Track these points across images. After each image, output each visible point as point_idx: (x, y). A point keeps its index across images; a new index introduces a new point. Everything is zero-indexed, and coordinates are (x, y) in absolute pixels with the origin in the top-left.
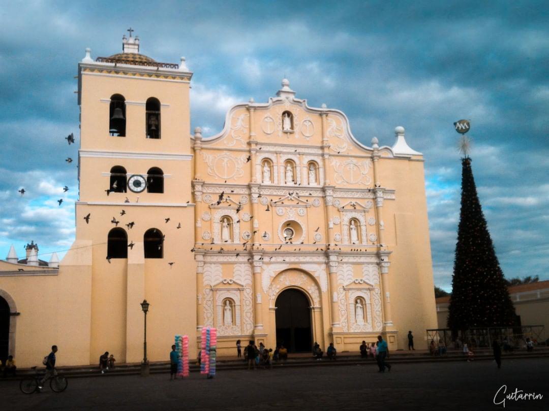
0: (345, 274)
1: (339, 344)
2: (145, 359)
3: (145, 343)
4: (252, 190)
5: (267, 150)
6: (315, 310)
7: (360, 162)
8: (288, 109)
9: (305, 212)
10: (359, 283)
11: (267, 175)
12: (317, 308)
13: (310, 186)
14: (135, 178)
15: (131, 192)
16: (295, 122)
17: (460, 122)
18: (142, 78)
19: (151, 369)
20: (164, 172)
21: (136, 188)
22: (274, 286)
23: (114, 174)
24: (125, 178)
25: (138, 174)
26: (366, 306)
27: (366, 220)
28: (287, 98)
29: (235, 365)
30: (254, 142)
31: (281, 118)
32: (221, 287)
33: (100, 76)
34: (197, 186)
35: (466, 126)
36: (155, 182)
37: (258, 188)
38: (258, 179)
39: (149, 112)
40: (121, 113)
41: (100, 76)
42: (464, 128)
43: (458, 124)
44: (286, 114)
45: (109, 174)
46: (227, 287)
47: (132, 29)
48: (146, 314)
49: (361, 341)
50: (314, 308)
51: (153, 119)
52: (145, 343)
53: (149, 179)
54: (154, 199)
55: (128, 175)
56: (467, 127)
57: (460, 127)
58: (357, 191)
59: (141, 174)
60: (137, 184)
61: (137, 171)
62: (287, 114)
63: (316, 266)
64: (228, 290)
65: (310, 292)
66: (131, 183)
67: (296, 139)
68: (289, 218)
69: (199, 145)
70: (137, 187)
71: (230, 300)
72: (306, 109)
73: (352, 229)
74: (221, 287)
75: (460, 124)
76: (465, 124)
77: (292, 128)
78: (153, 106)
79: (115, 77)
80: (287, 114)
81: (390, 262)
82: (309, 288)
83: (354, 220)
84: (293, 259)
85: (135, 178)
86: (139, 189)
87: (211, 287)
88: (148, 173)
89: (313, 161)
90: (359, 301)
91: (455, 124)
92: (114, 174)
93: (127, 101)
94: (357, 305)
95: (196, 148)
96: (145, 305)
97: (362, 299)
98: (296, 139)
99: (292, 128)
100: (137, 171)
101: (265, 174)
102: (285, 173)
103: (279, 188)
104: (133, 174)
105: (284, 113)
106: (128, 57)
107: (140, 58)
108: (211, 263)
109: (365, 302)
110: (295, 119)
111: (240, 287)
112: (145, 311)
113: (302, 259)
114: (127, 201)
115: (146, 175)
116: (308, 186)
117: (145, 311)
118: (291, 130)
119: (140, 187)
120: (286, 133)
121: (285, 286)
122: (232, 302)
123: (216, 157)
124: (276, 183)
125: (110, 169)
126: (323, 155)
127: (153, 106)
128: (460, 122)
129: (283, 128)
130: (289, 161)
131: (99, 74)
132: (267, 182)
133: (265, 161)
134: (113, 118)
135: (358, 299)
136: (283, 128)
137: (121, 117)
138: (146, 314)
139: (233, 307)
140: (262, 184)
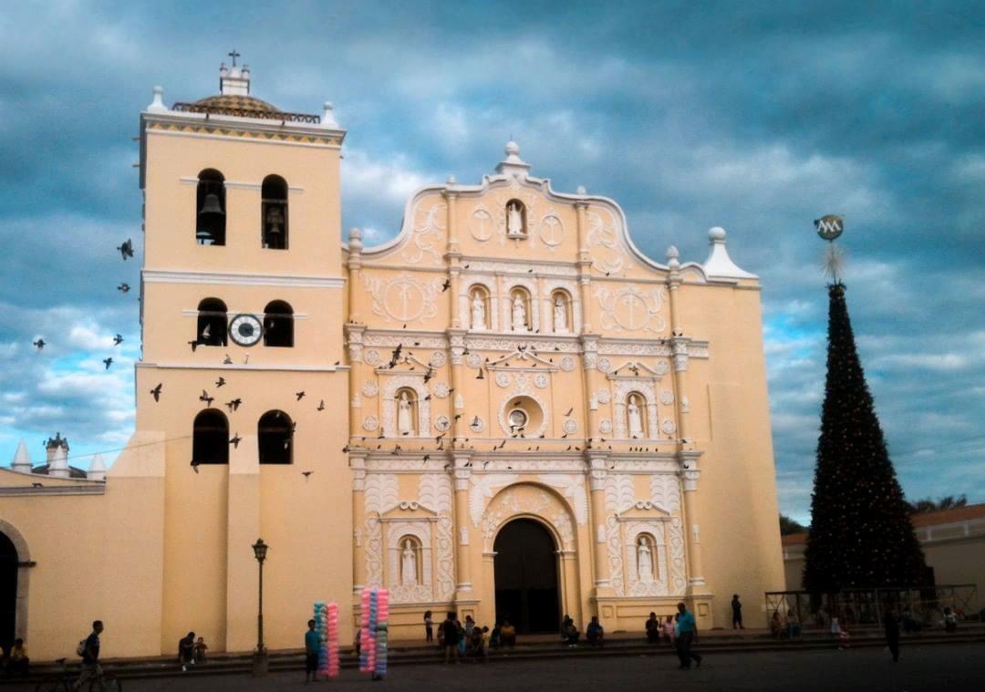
2: (260, 645)
3: (260, 617)
4: (452, 341)
5: (479, 269)
6: (566, 557)
9: (548, 380)
10: (644, 508)
11: (479, 314)
12: (569, 553)
14: (243, 320)
16: (529, 220)
17: (825, 219)
18: (254, 139)
19: (271, 664)
23: (204, 313)
24: (224, 320)
25: (248, 313)
26: (656, 550)
27: (657, 395)
28: (515, 176)
31: (504, 212)
34: (353, 334)
35: (837, 226)
36: (279, 327)
38: (462, 321)
40: (218, 203)
42: (832, 230)
43: (821, 222)
44: (514, 206)
45: (196, 313)
46: (408, 515)
47: (237, 52)
49: (647, 612)
50: (563, 554)
51: (275, 213)
52: (260, 617)
53: (267, 321)
54: (277, 357)
55: (230, 314)
56: (839, 229)
57: (826, 229)
58: (641, 342)
59: (253, 313)
60: (246, 330)
61: (246, 307)
62: (515, 204)
63: (567, 478)
65: (556, 525)
66: (235, 328)
67: (531, 250)
68: (519, 392)
69: (357, 261)
70: (246, 336)
72: (549, 196)
73: (631, 411)
75: (825, 222)
76: (835, 223)
77: (524, 229)
78: (274, 191)
80: (515, 204)
82: (554, 517)
83: (635, 396)
84: (526, 466)
85: (243, 320)
86: (249, 340)
87: (378, 515)
90: (643, 541)
91: (817, 223)
92: (204, 313)
93: (228, 181)
94: (641, 548)
95: (351, 267)
96: (260, 549)
98: (531, 250)
99: (524, 229)
100: (246, 307)
101: (475, 313)
104: (238, 313)
105: (509, 204)
106: (230, 103)
107: (250, 104)
108: (378, 473)
111: (431, 516)
112: (261, 559)
113: (541, 465)
114: (228, 362)
115: (261, 315)
116: (552, 334)
117: (261, 559)
118: (522, 234)
120: (513, 239)
123: (388, 281)
124: (494, 330)
126: (579, 279)
127: (274, 191)
128: (825, 219)
129: (508, 230)
130: (519, 290)
131: (178, 132)
132: (479, 327)
133: (476, 289)
134: (202, 212)
135: (642, 537)
136: (508, 230)
137: (218, 210)
139: (419, 552)
140: (470, 331)
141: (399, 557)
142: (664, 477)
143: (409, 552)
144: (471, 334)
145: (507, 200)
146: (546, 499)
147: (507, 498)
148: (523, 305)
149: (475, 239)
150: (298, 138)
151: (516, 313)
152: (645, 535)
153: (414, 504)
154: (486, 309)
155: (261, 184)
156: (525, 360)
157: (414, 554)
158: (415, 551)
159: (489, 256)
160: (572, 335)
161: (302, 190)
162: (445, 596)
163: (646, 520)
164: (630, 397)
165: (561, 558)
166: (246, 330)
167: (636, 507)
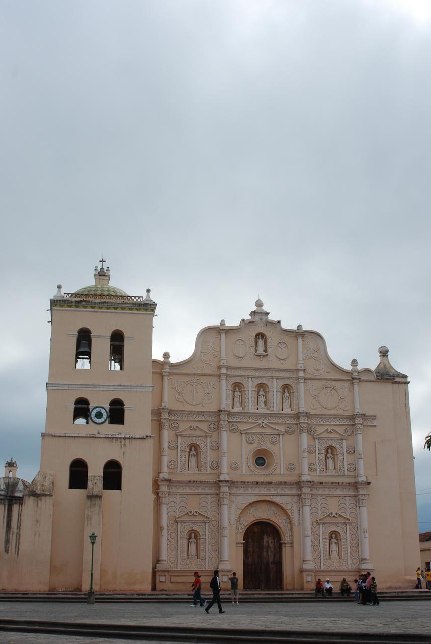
0: (348, 504)
1: (163, 582)
2: (91, 588)
3: (92, 573)
4: (221, 416)
5: (238, 374)
6: (287, 545)
7: (338, 385)
8: (260, 331)
11: (286, 403)
13: (260, 411)
15: (93, 423)
16: (268, 344)
18: (77, 309)
19: (96, 598)
20: (125, 403)
21: (100, 419)
22: (242, 519)
24: (88, 409)
25: (100, 406)
28: (261, 320)
29: (309, 598)
30: (223, 366)
31: (254, 340)
32: (185, 518)
33: (145, 314)
34: (163, 413)
36: (117, 413)
37: (169, 414)
39: (121, 343)
41: (145, 314)
44: (260, 336)
45: (73, 406)
46: (193, 519)
47: (104, 260)
48: (93, 545)
49: (341, 578)
50: (285, 543)
52: (92, 573)
53: (110, 410)
54: (115, 429)
55: (91, 407)
58: (336, 416)
59: (103, 406)
60: (99, 415)
61: (100, 402)
63: (288, 499)
64: (194, 523)
65: (281, 526)
68: (260, 447)
70: (98, 418)
71: (195, 532)
72: (280, 330)
74: (185, 518)
77: (265, 350)
79: (114, 313)
81: (368, 494)
83: (331, 449)
84: (263, 491)
86: (100, 420)
88: (109, 405)
89: (287, 385)
90: (334, 536)
93: (93, 333)
96: (93, 538)
97: (336, 533)
99: (265, 350)
100: (100, 402)
102: (258, 398)
103: (249, 415)
104: (95, 406)
105: (258, 335)
106: (97, 290)
108: (238, 495)
109: (341, 537)
110: (268, 341)
112: (93, 543)
115: (107, 407)
116: (282, 412)
117: (93, 543)
118: (264, 353)
119: (94, 416)
120: (259, 356)
121: (255, 519)
122: (339, 535)
125: (74, 401)
127: (117, 339)
132: (238, 408)
133: (236, 386)
134: (78, 351)
135: (333, 534)
137: (89, 351)
138: (93, 545)
139: (198, 540)
140: (232, 410)
141: (187, 543)
142: (347, 498)
143: (193, 540)
144: (233, 412)
145: (256, 333)
146: (264, 507)
147: (252, 510)
148: (264, 394)
149: (236, 356)
150: (116, 309)
151: (260, 400)
152: (334, 532)
153: (196, 512)
154: (290, 398)
155: (110, 335)
156: (195, 430)
157: (195, 541)
158: (196, 539)
159: (245, 366)
160: (292, 412)
161: (132, 337)
162: (210, 566)
163: (336, 524)
164: (328, 449)
165: (283, 545)
166: (99, 415)
167: (187, 513)
